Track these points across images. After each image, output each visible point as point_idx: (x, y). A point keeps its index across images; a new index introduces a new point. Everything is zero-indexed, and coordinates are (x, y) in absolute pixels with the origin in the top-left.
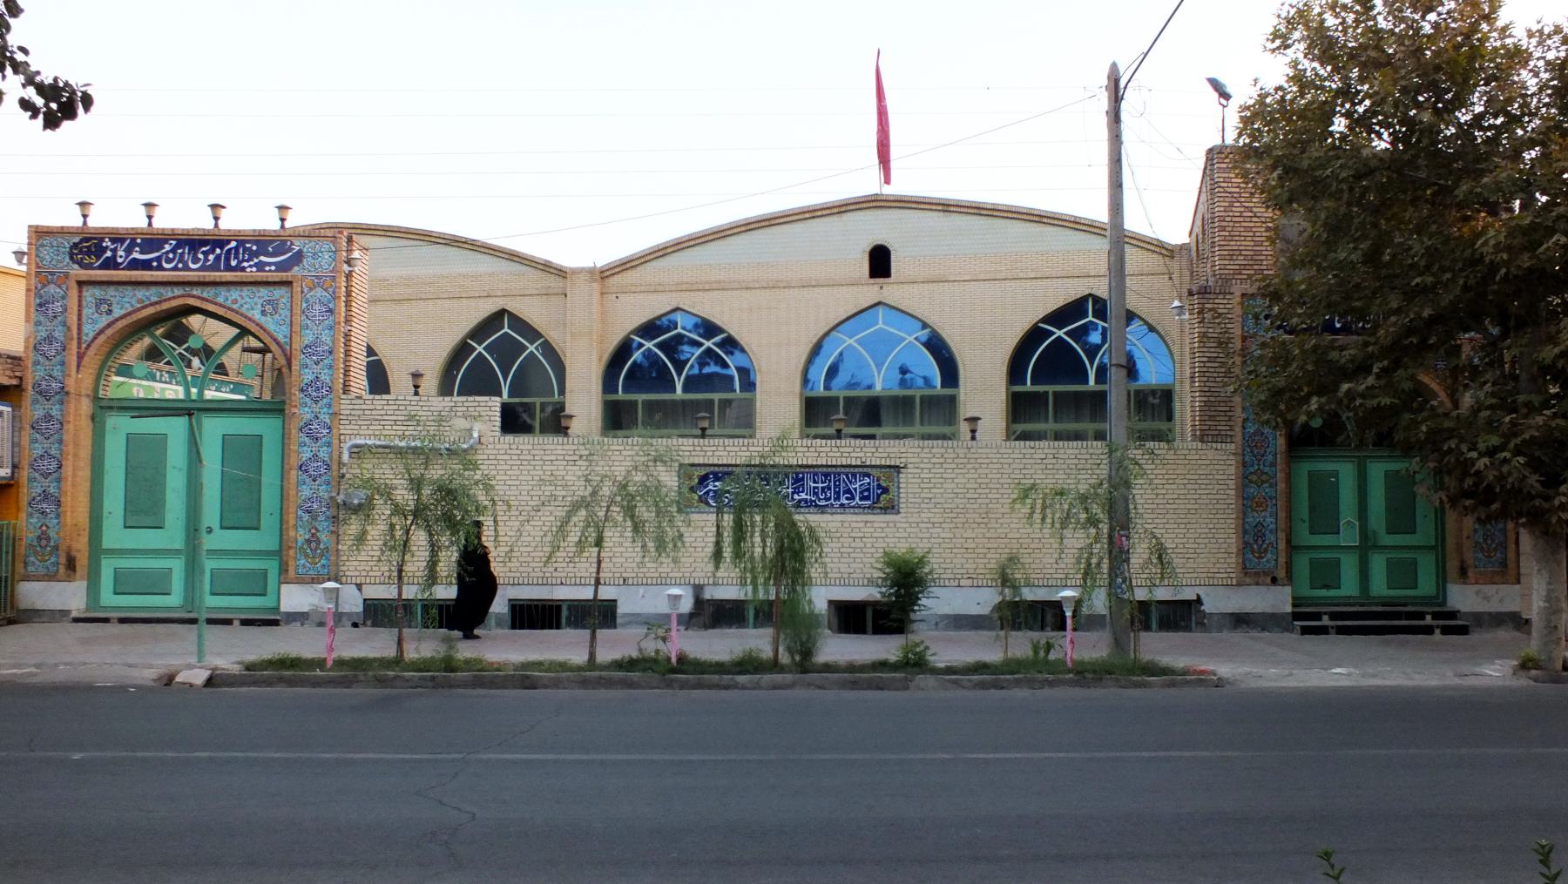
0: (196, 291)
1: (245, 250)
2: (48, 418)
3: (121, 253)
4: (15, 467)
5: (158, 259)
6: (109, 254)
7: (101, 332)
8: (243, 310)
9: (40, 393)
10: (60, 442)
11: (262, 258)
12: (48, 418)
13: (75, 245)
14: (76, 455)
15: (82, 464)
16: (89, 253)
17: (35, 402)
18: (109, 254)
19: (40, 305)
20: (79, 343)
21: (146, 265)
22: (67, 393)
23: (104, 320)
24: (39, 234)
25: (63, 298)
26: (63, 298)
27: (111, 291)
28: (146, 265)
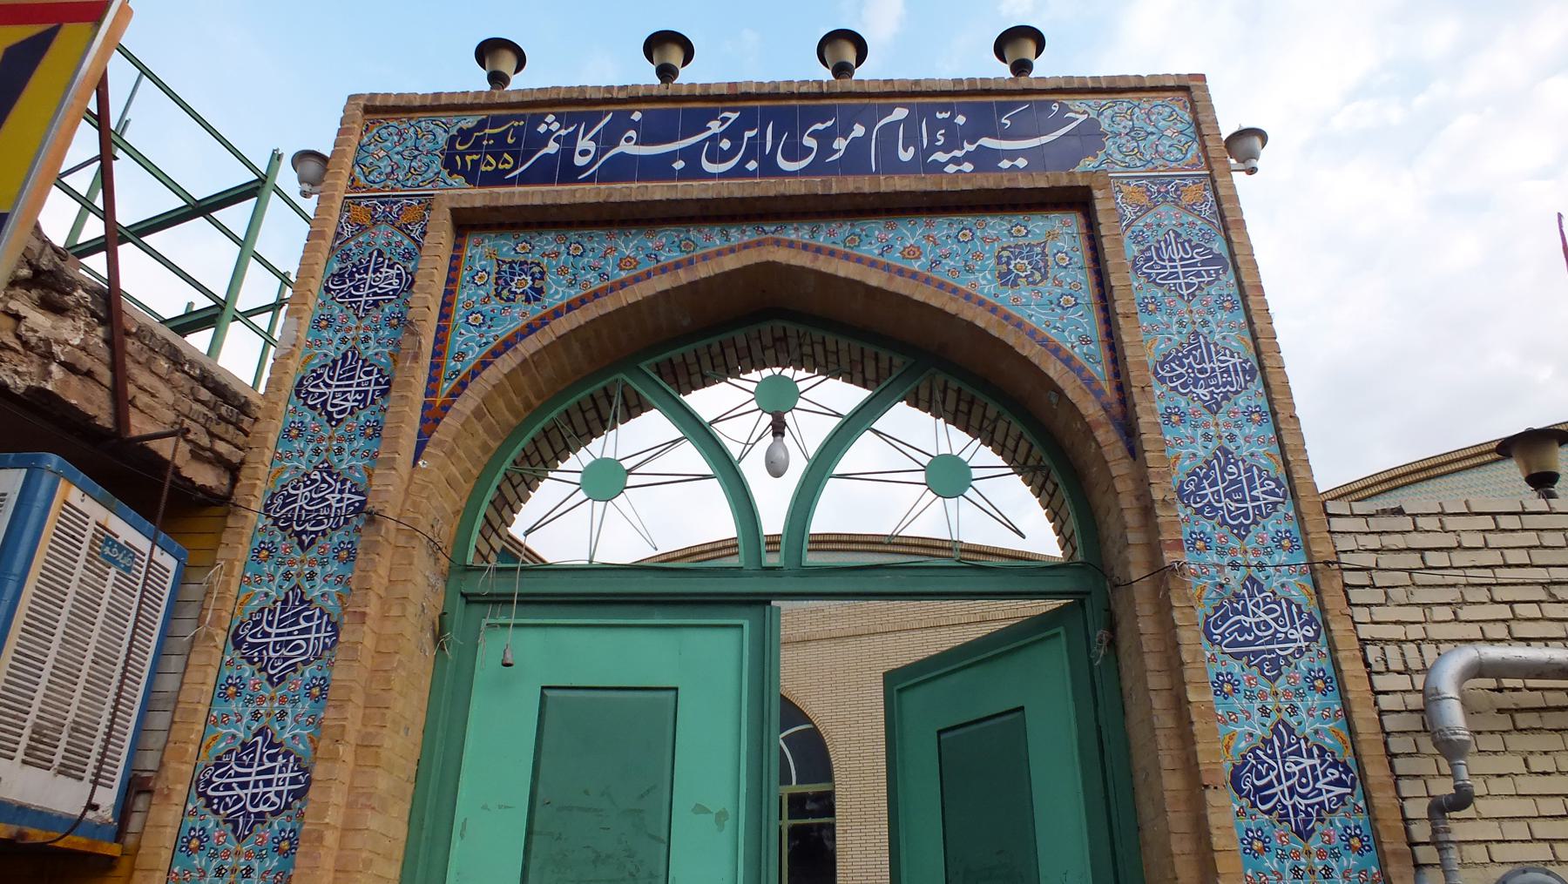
0: (798, 233)
1: (934, 126)
2: (295, 606)
3: (584, 143)
4: (136, 787)
5: (691, 154)
6: (552, 148)
7: (507, 345)
8: (940, 274)
9: (284, 524)
10: (321, 691)
11: (986, 142)
12: (295, 606)
13: (464, 135)
14: (366, 746)
15: (383, 783)
16: (499, 147)
17: (263, 552)
18: (552, 148)
19: (340, 276)
20: (433, 380)
21: (657, 168)
22: (373, 518)
23: (518, 315)
24: (374, 112)
25: (408, 256)
26: (408, 256)
27: (547, 242)
28: (657, 168)
